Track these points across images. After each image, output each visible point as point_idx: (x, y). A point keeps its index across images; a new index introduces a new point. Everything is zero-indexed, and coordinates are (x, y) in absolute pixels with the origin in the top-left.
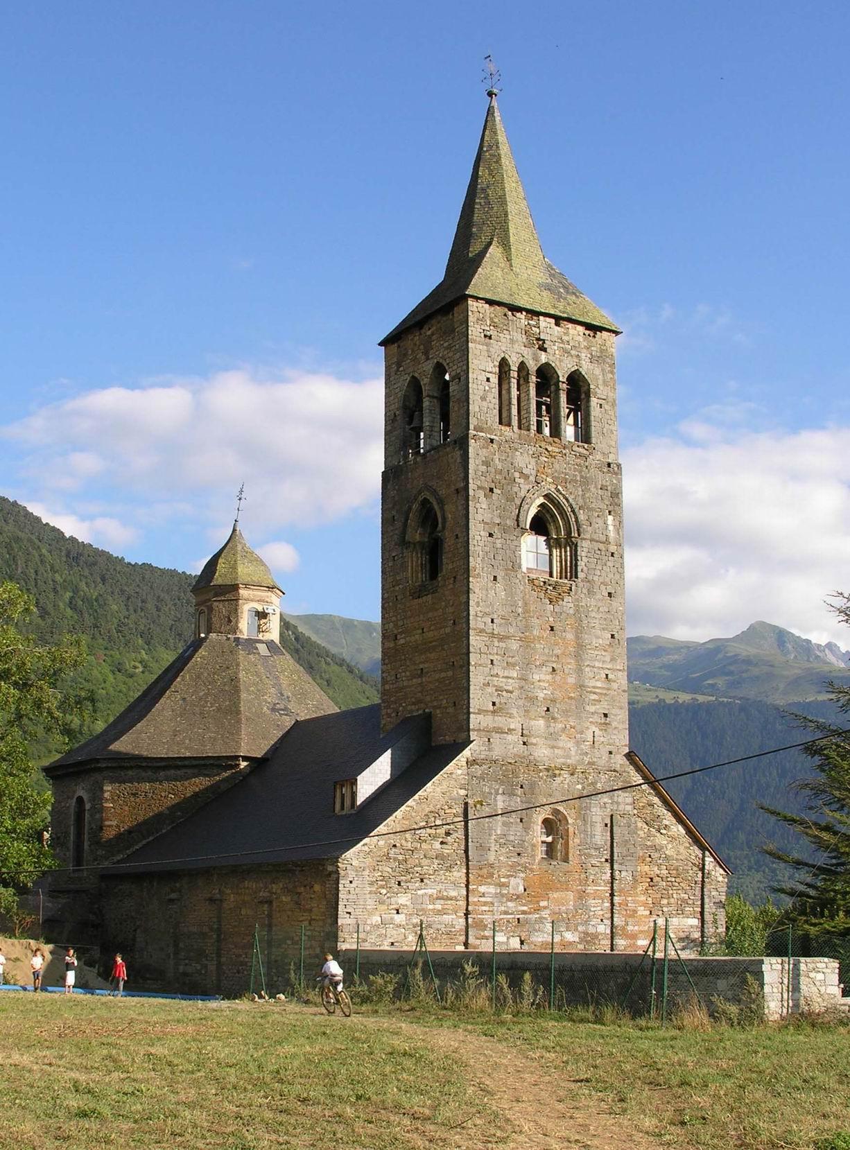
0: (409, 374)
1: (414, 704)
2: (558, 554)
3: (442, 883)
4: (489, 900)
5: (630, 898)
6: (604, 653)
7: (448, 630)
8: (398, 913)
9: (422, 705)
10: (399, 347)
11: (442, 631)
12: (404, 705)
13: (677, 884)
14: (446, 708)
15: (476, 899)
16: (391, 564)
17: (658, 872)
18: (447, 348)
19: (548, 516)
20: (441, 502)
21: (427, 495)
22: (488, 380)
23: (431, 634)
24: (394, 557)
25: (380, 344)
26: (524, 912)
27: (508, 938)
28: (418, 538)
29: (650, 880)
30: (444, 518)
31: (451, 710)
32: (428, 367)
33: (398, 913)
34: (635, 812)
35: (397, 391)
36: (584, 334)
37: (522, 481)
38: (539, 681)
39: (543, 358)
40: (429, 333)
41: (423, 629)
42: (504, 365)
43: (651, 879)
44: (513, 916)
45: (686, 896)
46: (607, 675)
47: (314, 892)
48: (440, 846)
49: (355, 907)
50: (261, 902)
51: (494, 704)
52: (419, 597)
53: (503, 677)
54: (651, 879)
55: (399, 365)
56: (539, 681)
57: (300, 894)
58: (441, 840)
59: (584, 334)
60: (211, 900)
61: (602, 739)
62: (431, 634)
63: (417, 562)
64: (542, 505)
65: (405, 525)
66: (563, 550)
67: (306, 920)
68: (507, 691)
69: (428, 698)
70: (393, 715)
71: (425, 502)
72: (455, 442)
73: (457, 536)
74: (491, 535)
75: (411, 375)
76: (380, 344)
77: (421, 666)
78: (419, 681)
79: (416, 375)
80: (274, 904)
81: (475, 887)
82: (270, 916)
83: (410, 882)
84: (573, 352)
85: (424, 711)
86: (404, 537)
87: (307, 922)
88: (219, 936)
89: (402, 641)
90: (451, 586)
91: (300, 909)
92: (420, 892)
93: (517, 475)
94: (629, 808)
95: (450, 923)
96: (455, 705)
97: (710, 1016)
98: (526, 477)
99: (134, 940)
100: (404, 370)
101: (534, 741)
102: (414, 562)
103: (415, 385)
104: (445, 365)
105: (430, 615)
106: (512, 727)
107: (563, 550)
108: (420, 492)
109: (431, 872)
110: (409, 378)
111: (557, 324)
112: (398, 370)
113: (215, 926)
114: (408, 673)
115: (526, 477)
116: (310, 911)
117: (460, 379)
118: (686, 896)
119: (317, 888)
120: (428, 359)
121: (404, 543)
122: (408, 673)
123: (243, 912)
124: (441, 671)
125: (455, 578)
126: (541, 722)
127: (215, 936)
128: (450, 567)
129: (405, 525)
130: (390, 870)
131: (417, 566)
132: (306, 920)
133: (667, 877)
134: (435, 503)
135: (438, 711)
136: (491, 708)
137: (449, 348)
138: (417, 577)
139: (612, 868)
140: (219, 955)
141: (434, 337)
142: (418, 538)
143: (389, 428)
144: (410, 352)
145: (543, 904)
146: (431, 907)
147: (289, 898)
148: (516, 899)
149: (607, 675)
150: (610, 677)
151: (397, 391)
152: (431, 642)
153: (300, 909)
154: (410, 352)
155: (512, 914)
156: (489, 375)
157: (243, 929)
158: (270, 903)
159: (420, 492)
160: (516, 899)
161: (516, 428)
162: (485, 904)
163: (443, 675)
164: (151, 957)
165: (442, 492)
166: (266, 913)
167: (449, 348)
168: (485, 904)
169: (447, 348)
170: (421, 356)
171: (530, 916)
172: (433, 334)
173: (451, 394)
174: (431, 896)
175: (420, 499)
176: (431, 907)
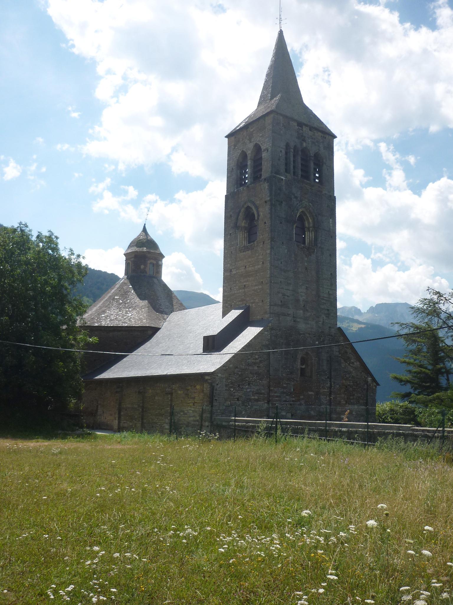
0: (240, 150)
1: (240, 301)
2: (308, 235)
3: (258, 386)
4: (279, 395)
5: (338, 396)
6: (327, 281)
7: (259, 266)
8: (238, 400)
9: (245, 302)
10: (235, 138)
11: (256, 267)
12: (235, 302)
13: (356, 389)
14: (258, 303)
15: (273, 394)
16: (229, 237)
17: (349, 383)
18: (261, 137)
19: (305, 217)
20: (257, 208)
21: (249, 204)
22: (281, 151)
23: (250, 269)
24: (231, 234)
25: (226, 137)
26: (293, 401)
27: (286, 413)
28: (243, 224)
29: (345, 387)
30: (259, 215)
31: (260, 304)
32: (251, 146)
33: (238, 400)
34: (340, 355)
35: (234, 158)
36: (321, 136)
37: (295, 200)
38: (301, 292)
39: (304, 145)
40: (252, 130)
41: (246, 267)
42: (287, 146)
43: (346, 387)
44: (288, 403)
45: (360, 395)
46: (329, 292)
47: (196, 389)
48: (257, 368)
49: (219, 397)
50: (167, 394)
51: (281, 302)
52: (244, 252)
53: (285, 289)
54: (346, 387)
55: (235, 146)
56: (301, 292)
57: (188, 390)
58: (257, 365)
59: (321, 136)
60: (139, 392)
61: (326, 321)
62: (250, 269)
63: (242, 236)
64: (302, 211)
65: (237, 219)
66: (310, 233)
67: (192, 403)
68: (288, 296)
69: (248, 299)
70: (229, 307)
71: (248, 208)
72: (265, 179)
73: (265, 223)
74: (281, 223)
75: (242, 150)
76: (226, 137)
77: (244, 284)
78: (243, 290)
79: (244, 150)
80: (174, 395)
81: (272, 388)
82: (171, 400)
83: (244, 385)
84: (316, 144)
85: (246, 305)
86: (237, 223)
87: (192, 404)
88: (143, 410)
89: (234, 272)
90: (261, 246)
91: (188, 397)
92: (248, 390)
93: (293, 197)
94: (337, 353)
95: (261, 405)
96: (263, 302)
97: (188, 423)
98: (296, 197)
99: (97, 410)
100: (238, 148)
101: (298, 320)
102: (241, 237)
103: (244, 155)
104: (260, 144)
105: (250, 260)
106: (289, 313)
107: (310, 233)
108: (245, 203)
109: (253, 380)
110: (240, 152)
111: (310, 130)
112: (234, 148)
113: (141, 405)
114: (237, 287)
115: (296, 197)
116: (194, 398)
117: (268, 150)
118: (360, 395)
119: (198, 387)
120: (251, 142)
121: (236, 227)
122: (237, 287)
123: (156, 398)
124: (256, 286)
125: (264, 242)
126: (301, 311)
127: (141, 410)
128: (261, 237)
129: (237, 219)
130: (235, 379)
131: (242, 238)
132: (192, 403)
133: (353, 386)
134: (253, 208)
135: (253, 305)
136: (280, 303)
137: (262, 136)
138: (242, 243)
139: (330, 381)
140: (142, 419)
141: (254, 132)
142: (243, 224)
143: (229, 175)
144: (241, 140)
145: (302, 397)
146: (253, 397)
147: (182, 392)
148: (290, 394)
149: (329, 292)
150: (330, 292)
151: (234, 158)
152: (250, 272)
153: (188, 397)
154: (241, 140)
155: (288, 402)
156: (282, 149)
157: (156, 406)
158: (171, 394)
159: (245, 203)
160: (290, 394)
161: (292, 175)
162: (277, 397)
163: (256, 287)
164: (106, 419)
165: (258, 203)
166: (170, 399)
167: (262, 136)
168: (277, 397)
169: (261, 137)
170: (247, 141)
171: (296, 403)
172: (254, 131)
173: (263, 157)
174: (253, 392)
175: (245, 206)
176: (253, 397)
